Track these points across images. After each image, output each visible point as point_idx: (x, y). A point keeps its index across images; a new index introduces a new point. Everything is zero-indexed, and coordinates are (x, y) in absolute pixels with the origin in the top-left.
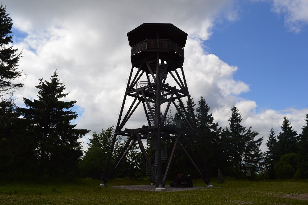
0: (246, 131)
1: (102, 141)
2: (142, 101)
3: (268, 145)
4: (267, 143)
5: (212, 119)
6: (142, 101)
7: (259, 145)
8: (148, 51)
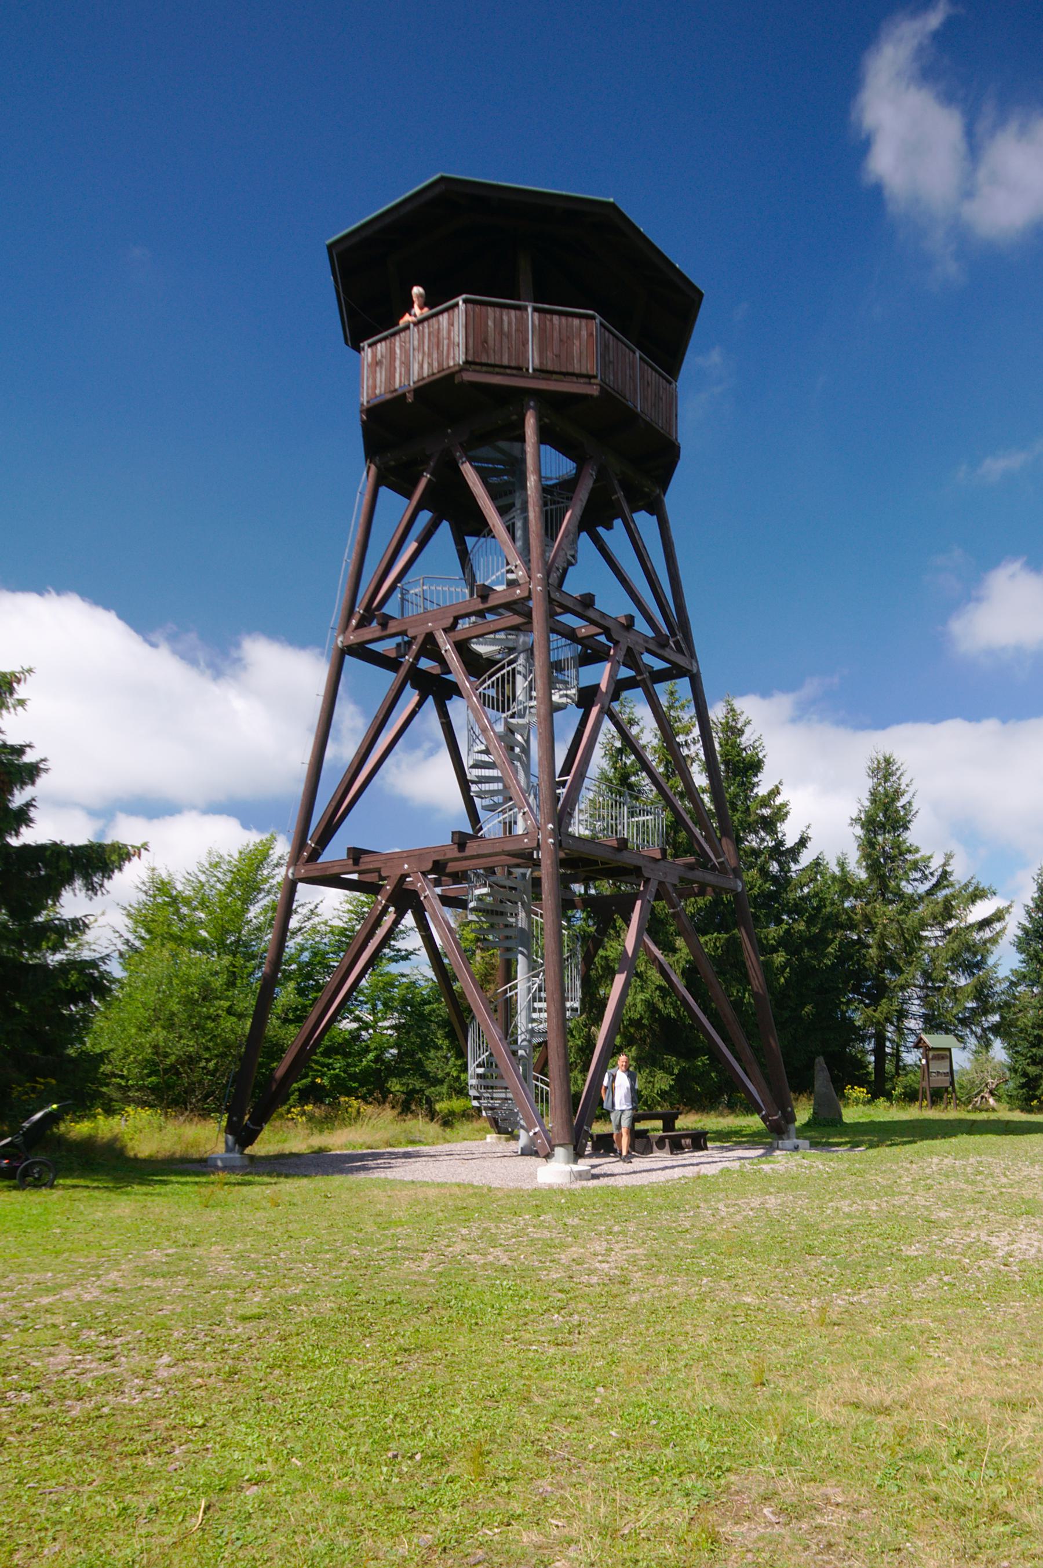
0: (932, 874)
1: (29, 874)
2: (431, 697)
3: (1020, 949)
4: (1020, 933)
5: (781, 814)
6: (431, 697)
7: (994, 940)
8: (468, 376)
